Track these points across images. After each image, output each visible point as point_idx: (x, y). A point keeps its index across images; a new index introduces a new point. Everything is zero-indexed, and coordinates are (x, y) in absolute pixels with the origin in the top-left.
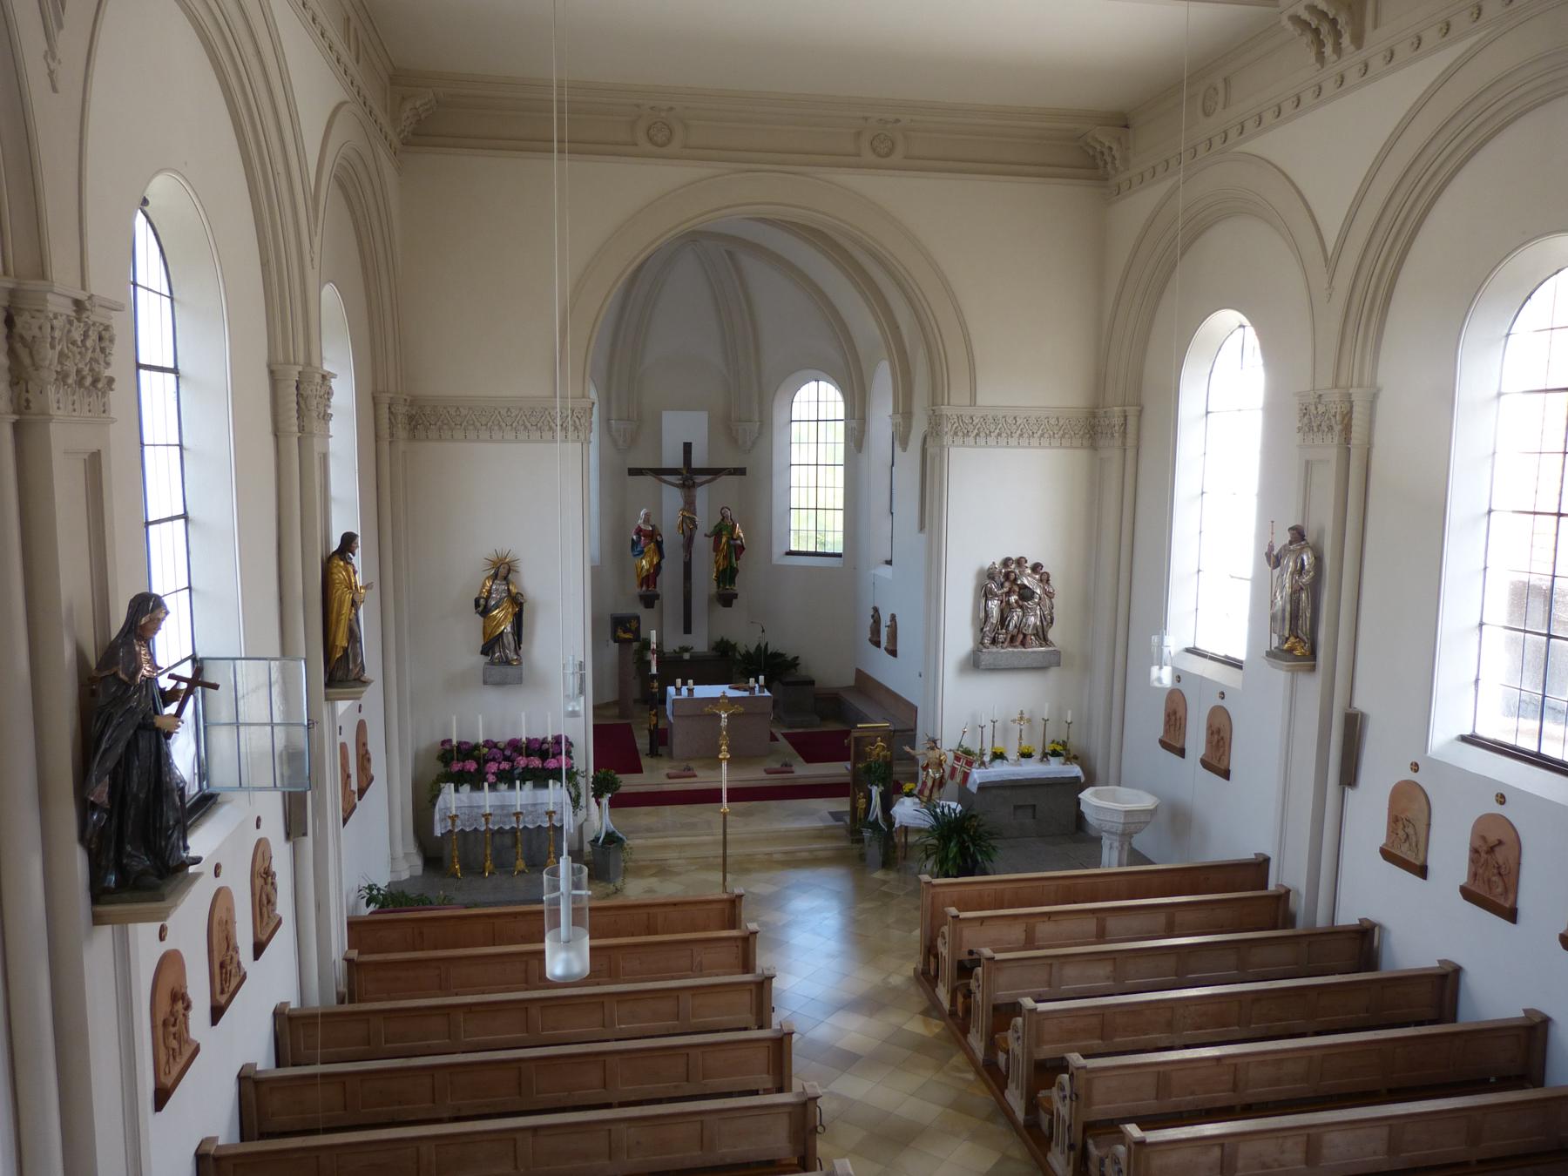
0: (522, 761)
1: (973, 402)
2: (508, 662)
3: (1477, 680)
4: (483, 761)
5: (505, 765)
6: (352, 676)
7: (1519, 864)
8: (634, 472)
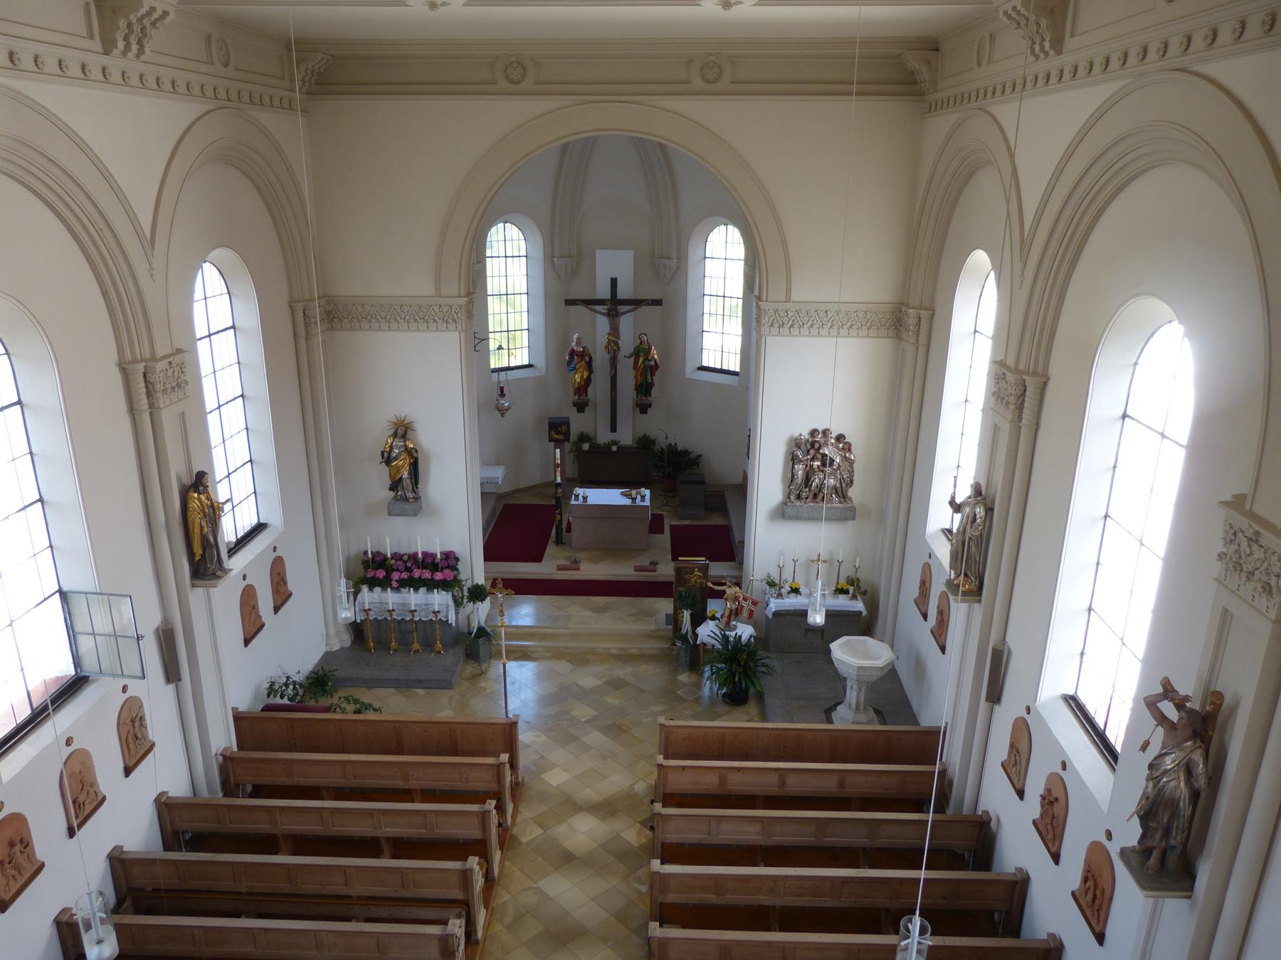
0: (417, 573)
1: (788, 300)
2: (406, 499)
3: (1082, 654)
4: (390, 570)
5: (405, 575)
6: (210, 572)
7: (1065, 822)
8: (570, 302)
